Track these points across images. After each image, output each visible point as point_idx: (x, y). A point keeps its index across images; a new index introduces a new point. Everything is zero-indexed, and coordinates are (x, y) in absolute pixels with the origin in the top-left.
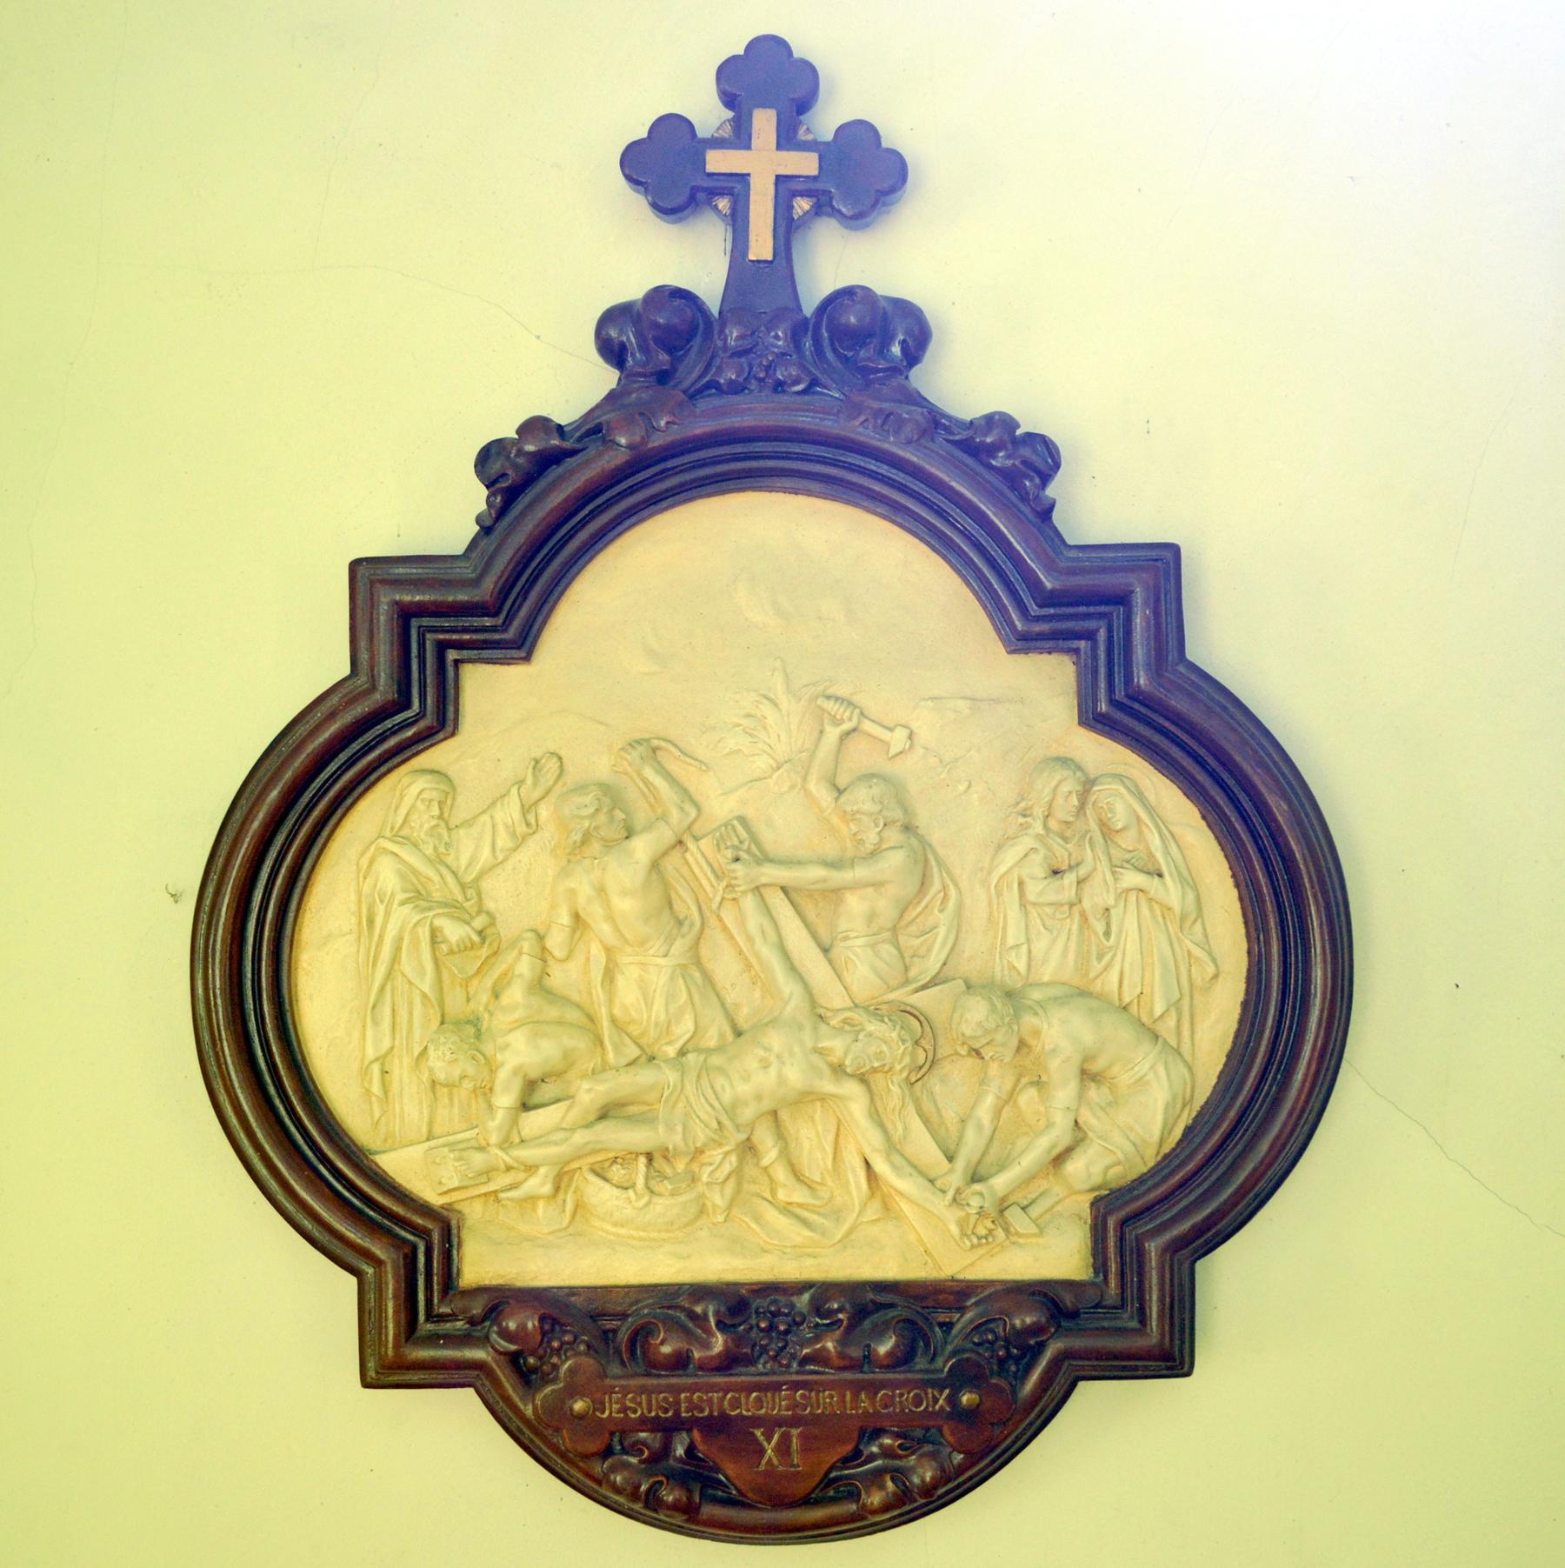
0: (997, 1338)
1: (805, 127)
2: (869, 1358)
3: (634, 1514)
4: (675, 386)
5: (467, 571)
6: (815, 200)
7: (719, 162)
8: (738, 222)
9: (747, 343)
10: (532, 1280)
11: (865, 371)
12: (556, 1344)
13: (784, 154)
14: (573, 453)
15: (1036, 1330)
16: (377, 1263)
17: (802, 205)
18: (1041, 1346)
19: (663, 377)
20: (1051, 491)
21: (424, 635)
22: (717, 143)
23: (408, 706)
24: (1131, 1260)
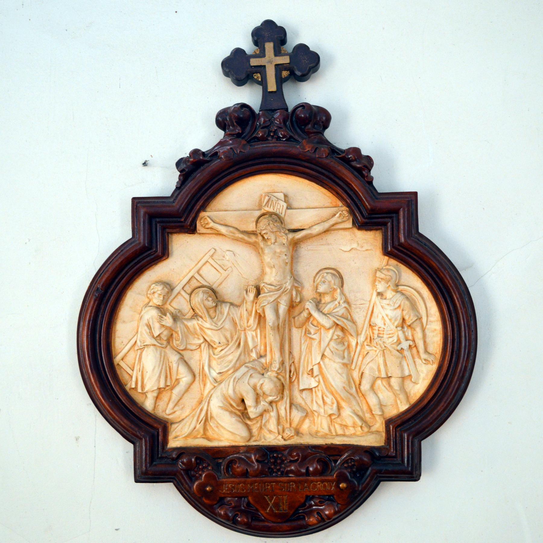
2: (308, 473)
7: (254, 62)
8: (263, 83)
13: (278, 58)
14: (207, 162)
17: (285, 74)
19: (239, 135)
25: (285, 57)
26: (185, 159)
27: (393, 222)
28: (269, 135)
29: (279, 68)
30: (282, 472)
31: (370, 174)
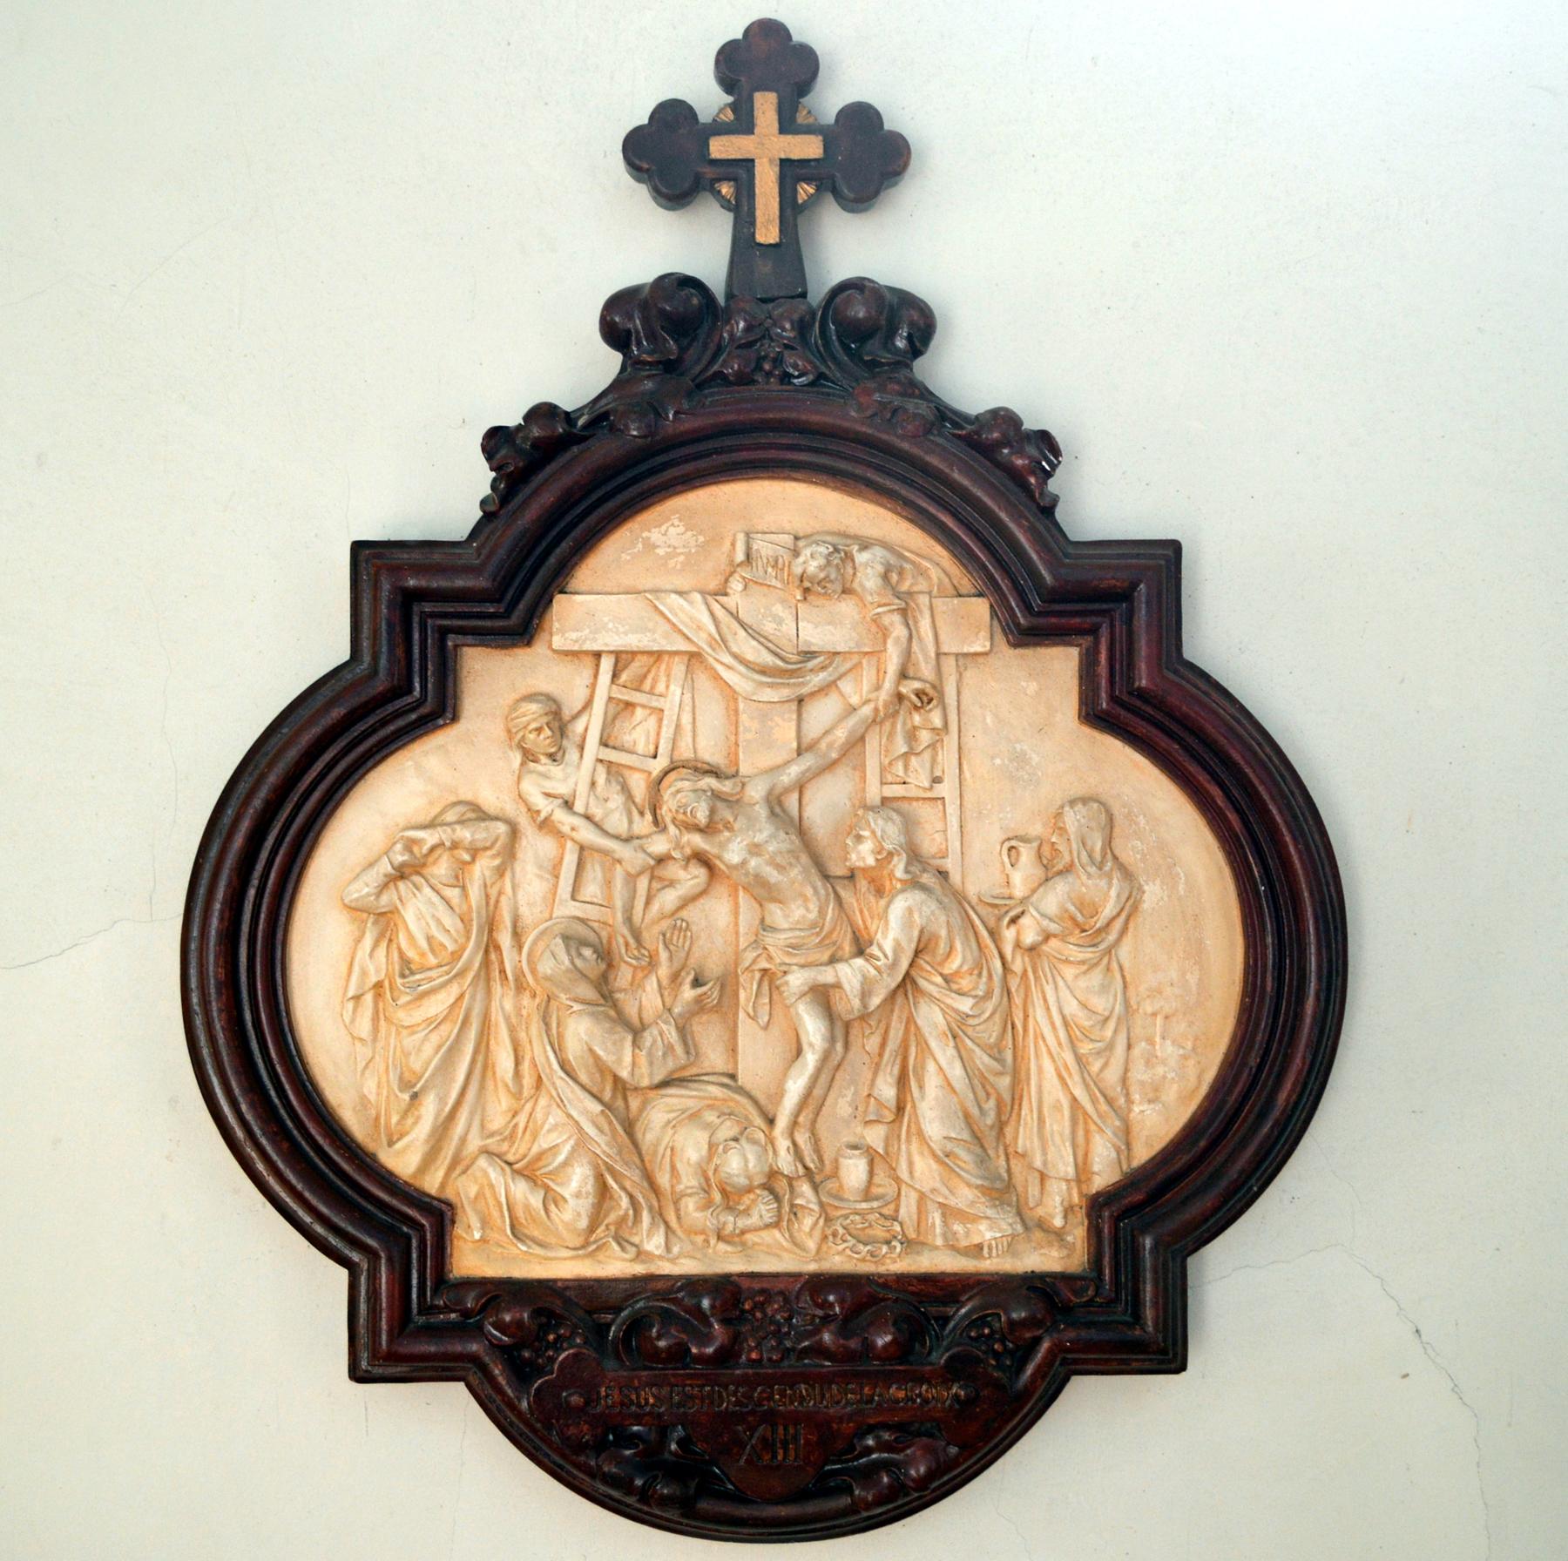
0: (993, 1332)
3: (622, 1508)
4: (682, 374)
5: (469, 557)
7: (720, 148)
8: (742, 211)
10: (1196, 952)
11: (873, 365)
12: (551, 1337)
17: (805, 190)
18: (1037, 1341)
19: (670, 367)
20: (1053, 485)
22: (718, 128)
23: (410, 691)
25: (812, 138)
27: (1112, 626)
28: (759, 368)
29: (791, 171)
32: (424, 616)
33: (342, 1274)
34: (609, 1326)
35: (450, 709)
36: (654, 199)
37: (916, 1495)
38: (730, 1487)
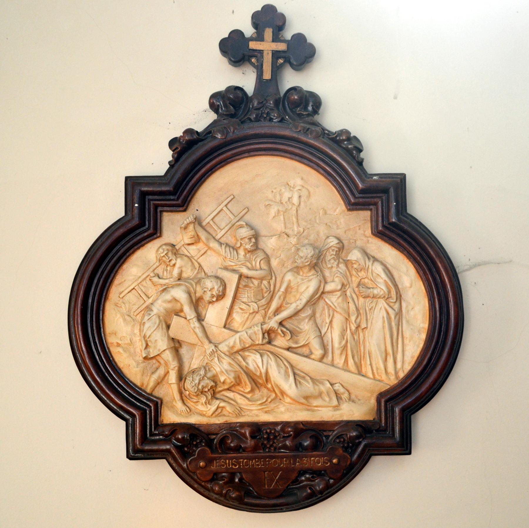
0: (344, 440)
1: (281, 35)
6: (285, 59)
7: (253, 45)
9: (260, 105)
14: (202, 140)
15: (357, 437)
16: (133, 416)
17: (281, 61)
18: (360, 443)
20: (362, 155)
21: (150, 202)
23: (145, 225)
24: (389, 414)
26: (178, 138)
28: (262, 116)
29: (276, 55)
30: (275, 448)
31: (360, 155)
32: (150, 200)
33: (123, 423)
34: (214, 439)
35: (159, 232)
36: (230, 64)
37: (320, 496)
38: (255, 494)
